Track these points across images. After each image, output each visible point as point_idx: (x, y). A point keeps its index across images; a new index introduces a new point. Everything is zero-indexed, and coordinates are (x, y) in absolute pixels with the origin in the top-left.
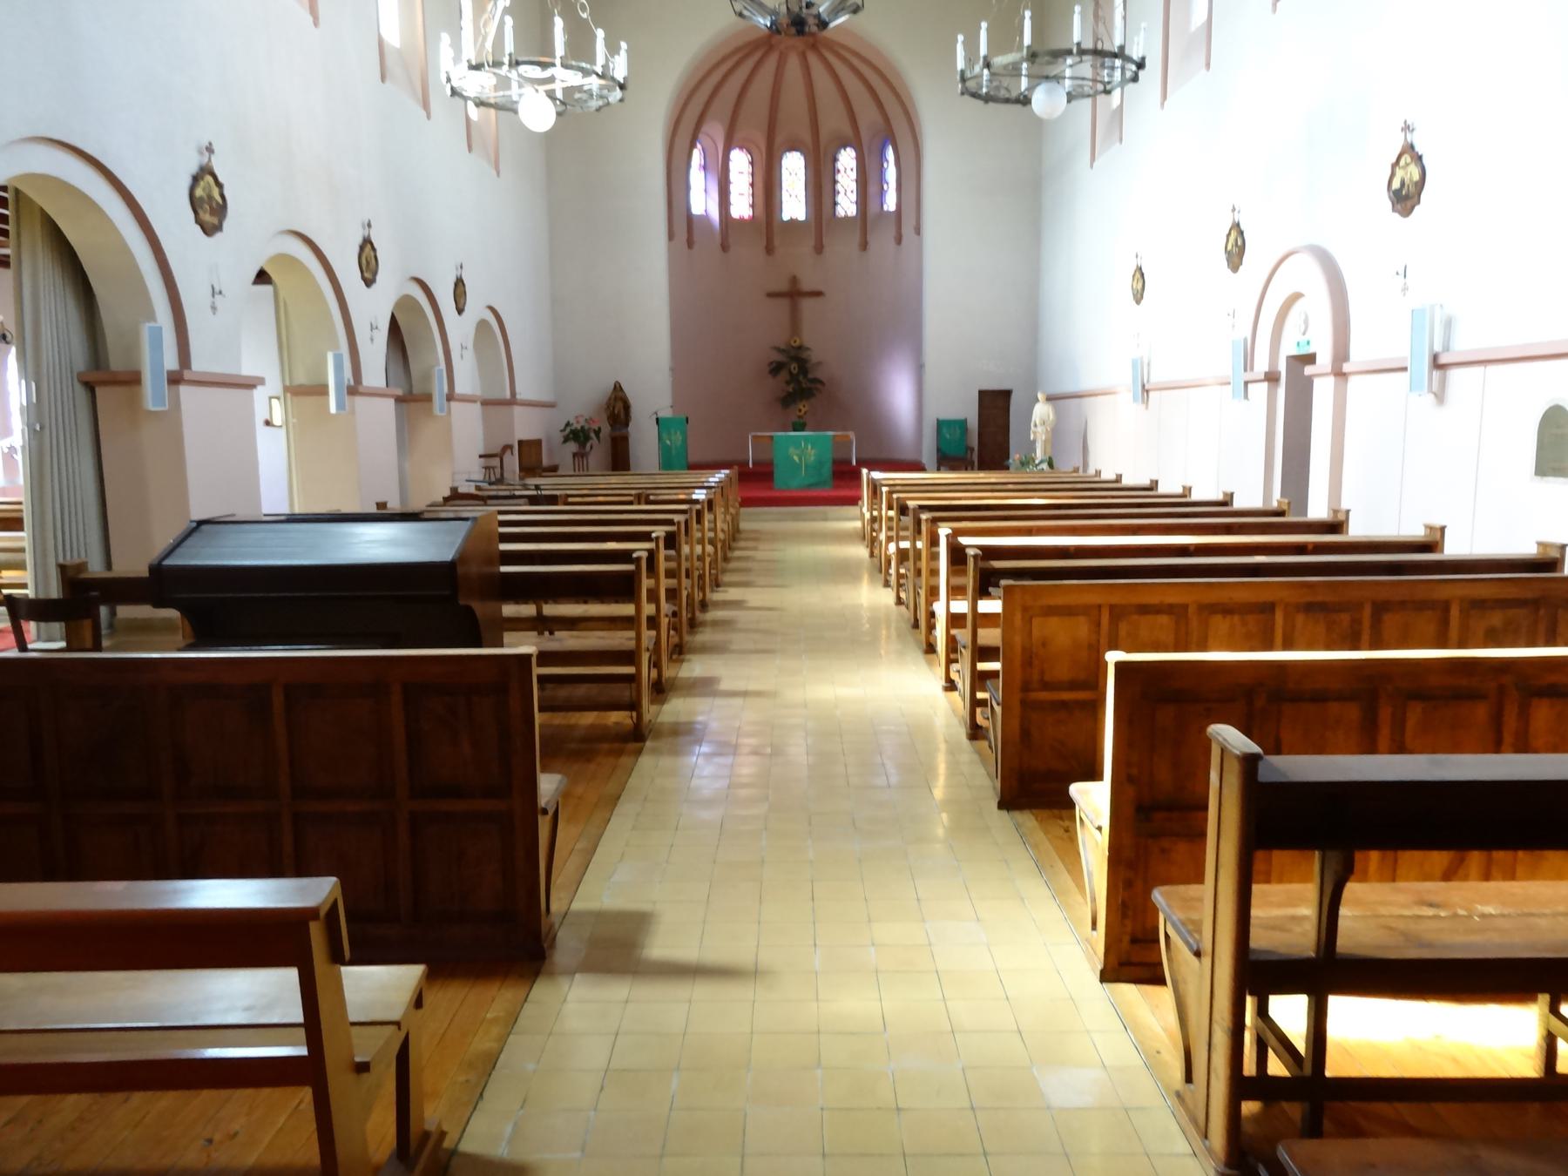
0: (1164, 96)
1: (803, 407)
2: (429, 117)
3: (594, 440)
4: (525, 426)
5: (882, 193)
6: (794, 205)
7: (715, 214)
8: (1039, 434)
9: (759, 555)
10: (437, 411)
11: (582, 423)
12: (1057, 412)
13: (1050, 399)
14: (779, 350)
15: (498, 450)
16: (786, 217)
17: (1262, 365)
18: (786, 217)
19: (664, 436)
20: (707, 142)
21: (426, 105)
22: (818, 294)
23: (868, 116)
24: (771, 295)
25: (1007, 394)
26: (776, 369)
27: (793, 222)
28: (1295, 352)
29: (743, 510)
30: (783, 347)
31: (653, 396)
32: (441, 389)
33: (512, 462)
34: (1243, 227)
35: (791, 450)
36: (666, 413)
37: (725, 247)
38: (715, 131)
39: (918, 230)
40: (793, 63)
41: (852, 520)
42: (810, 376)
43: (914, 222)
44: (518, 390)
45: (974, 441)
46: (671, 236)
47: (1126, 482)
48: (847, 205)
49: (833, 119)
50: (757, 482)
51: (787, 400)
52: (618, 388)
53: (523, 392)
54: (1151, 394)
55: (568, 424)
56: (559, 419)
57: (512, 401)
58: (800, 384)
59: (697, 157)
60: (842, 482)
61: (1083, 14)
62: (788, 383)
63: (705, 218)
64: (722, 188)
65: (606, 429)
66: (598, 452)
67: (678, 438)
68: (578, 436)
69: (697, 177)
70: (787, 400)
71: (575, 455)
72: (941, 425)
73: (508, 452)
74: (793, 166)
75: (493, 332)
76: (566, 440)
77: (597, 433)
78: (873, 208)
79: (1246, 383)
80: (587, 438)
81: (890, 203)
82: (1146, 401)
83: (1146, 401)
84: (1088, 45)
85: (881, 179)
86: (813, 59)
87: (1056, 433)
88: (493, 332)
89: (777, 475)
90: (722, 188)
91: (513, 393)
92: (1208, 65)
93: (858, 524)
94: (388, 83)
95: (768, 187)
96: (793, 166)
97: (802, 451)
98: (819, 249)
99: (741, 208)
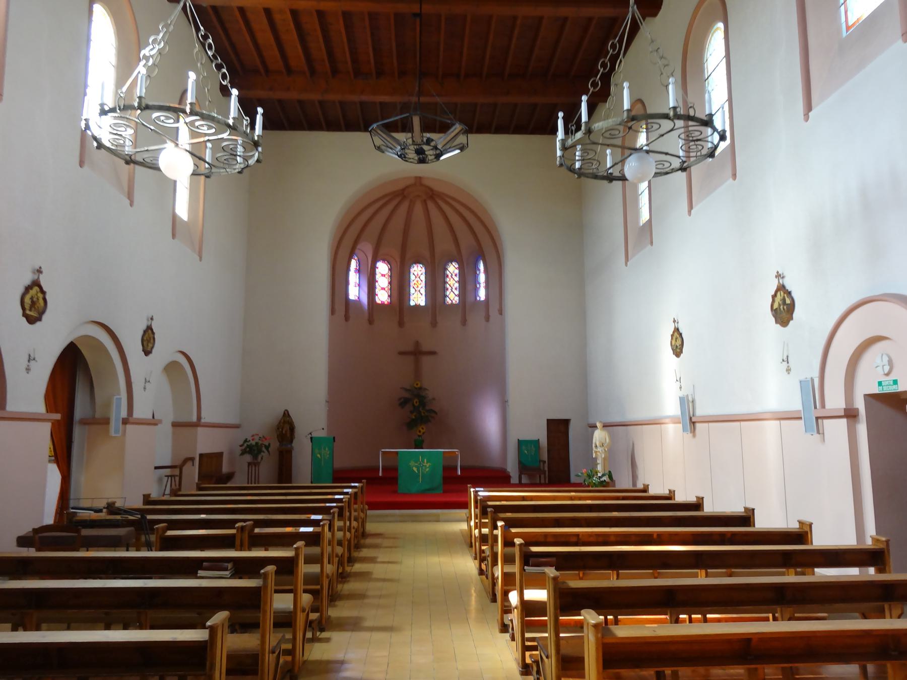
0: (691, 207)
1: (422, 429)
2: (131, 205)
3: (265, 454)
4: (206, 442)
5: (476, 290)
6: (418, 297)
7: (365, 299)
8: (599, 453)
9: (377, 570)
10: (112, 433)
11: (257, 440)
12: (611, 436)
13: (605, 426)
14: (406, 390)
15: (178, 463)
16: (412, 303)
17: (835, 401)
18: (412, 303)
19: (317, 451)
20: (362, 255)
21: (130, 196)
22: (433, 353)
23: (466, 240)
24: (401, 353)
25: (566, 423)
26: (404, 402)
27: (417, 307)
28: (876, 390)
29: (369, 512)
30: (408, 388)
31: (313, 419)
32: (118, 412)
33: (192, 473)
34: (788, 288)
35: (412, 463)
36: (321, 434)
37: (371, 321)
38: (366, 248)
39: (501, 312)
40: (418, 209)
41: (460, 523)
42: (427, 408)
43: (498, 307)
44: (203, 415)
45: (545, 457)
46: (333, 311)
47: (709, 508)
48: (453, 297)
49: (444, 243)
50: (383, 488)
51: (411, 424)
52: (286, 414)
53: (206, 417)
54: (698, 425)
55: (246, 441)
56: (239, 437)
57: (198, 424)
58: (421, 413)
59: (354, 264)
60: (450, 491)
61: (675, 83)
62: (412, 412)
63: (358, 302)
64: (370, 284)
65: (275, 445)
66: (267, 465)
67: (326, 452)
68: (252, 449)
69: (353, 277)
70: (411, 424)
71: (249, 464)
72: (520, 443)
73: (189, 464)
74: (418, 273)
75: (181, 372)
76: (243, 453)
77: (267, 447)
78: (470, 299)
79: (817, 418)
80: (260, 451)
81: (482, 294)
82: (693, 431)
83: (693, 431)
84: (681, 111)
85: (476, 276)
86: (431, 205)
87: (611, 454)
88: (181, 372)
89: (400, 481)
90: (370, 284)
91: (199, 417)
92: (734, 176)
93: (464, 526)
94: (86, 167)
95: (400, 285)
96: (418, 273)
97: (421, 463)
98: (434, 324)
99: (382, 297)
